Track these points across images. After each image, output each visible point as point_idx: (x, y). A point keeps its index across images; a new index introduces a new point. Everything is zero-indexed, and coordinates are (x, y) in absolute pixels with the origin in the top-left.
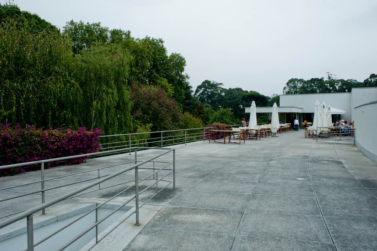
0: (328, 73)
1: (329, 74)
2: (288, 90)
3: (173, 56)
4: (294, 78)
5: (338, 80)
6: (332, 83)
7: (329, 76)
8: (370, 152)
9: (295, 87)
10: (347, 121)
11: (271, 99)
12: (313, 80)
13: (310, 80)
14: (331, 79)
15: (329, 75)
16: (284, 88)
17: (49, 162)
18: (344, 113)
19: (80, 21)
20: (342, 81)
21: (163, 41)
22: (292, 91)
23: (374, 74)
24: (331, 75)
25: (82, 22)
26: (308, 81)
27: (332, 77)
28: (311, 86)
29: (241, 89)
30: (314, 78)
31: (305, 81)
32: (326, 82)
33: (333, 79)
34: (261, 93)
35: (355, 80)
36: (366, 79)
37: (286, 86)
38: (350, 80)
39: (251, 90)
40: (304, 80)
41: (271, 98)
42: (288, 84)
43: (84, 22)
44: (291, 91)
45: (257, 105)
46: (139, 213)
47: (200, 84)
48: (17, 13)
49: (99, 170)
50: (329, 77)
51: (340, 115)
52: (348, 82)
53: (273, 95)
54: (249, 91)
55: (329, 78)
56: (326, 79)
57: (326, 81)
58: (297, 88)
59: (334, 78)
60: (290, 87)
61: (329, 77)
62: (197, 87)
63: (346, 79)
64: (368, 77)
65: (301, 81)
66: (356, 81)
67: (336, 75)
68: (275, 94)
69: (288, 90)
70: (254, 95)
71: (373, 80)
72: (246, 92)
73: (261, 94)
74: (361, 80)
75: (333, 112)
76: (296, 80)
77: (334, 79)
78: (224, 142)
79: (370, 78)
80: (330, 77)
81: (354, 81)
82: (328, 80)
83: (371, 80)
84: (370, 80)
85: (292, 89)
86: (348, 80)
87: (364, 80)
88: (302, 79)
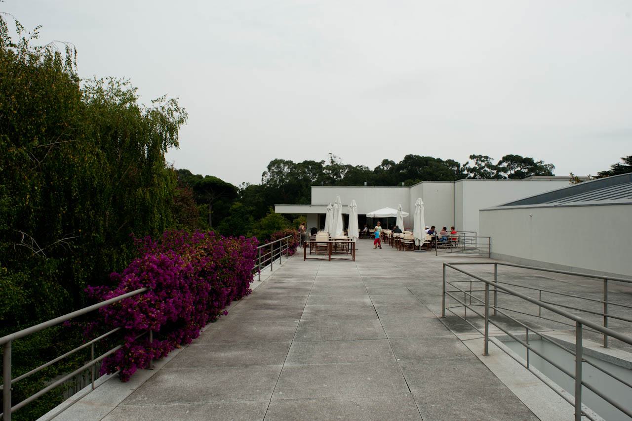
0: (331, 154)
1: (332, 156)
4: (279, 158)
5: (343, 166)
6: (336, 168)
8: (12, 399)
9: (280, 173)
10: (452, 226)
11: (239, 189)
12: (306, 164)
13: (302, 162)
14: (335, 163)
16: (264, 174)
18: (407, 215)
20: (349, 166)
23: (387, 160)
24: (335, 157)
26: (299, 164)
27: (336, 161)
28: (305, 172)
29: (188, 171)
30: (308, 160)
32: (328, 168)
33: (337, 164)
34: (226, 180)
35: (366, 167)
37: (267, 170)
38: (360, 166)
39: (207, 175)
40: (389, 160)
41: (240, 188)
42: (269, 167)
44: (275, 179)
46: (576, 361)
47: (477, 154)
49: (496, 264)
50: (332, 160)
52: (358, 170)
53: (241, 184)
54: (204, 176)
55: (332, 162)
57: (328, 166)
59: (339, 162)
61: (332, 160)
62: (450, 160)
64: (380, 164)
65: (289, 163)
66: (367, 168)
67: (341, 158)
70: (216, 184)
71: (385, 168)
72: (200, 177)
73: (226, 182)
75: (393, 215)
76: (282, 161)
77: (339, 164)
78: (352, 259)
79: (383, 165)
81: (365, 168)
83: (384, 168)
84: (382, 167)
86: (356, 167)
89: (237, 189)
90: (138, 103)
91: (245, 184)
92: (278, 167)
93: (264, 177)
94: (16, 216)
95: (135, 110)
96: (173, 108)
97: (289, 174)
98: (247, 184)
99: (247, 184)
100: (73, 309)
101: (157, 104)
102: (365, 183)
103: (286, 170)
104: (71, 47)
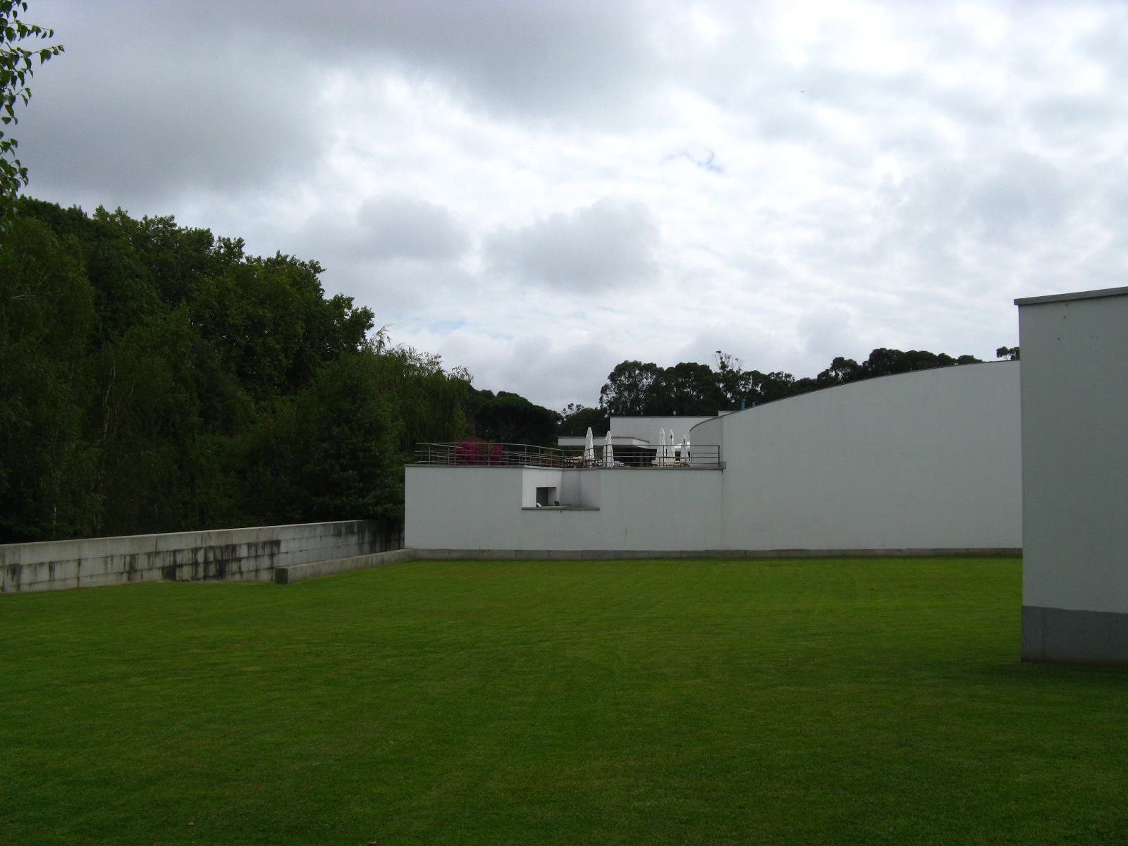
0: (719, 352)
2: (615, 395)
3: (341, 303)
4: (631, 360)
7: (723, 360)
9: (633, 387)
11: (561, 418)
15: (721, 358)
17: (503, 464)
19: (116, 209)
21: (319, 267)
22: (625, 397)
24: (729, 358)
25: (123, 210)
31: (662, 369)
36: (823, 370)
37: (609, 382)
41: (564, 415)
42: (613, 377)
43: (127, 212)
45: (595, 435)
48: (53, 210)
51: (1022, 558)
54: (495, 394)
55: (723, 366)
56: (715, 368)
58: (639, 390)
59: (734, 366)
60: (619, 387)
61: (722, 363)
63: (765, 371)
64: (829, 367)
65: (650, 368)
68: (575, 405)
69: (615, 395)
72: (488, 394)
74: (812, 369)
76: (636, 365)
77: (735, 370)
80: (726, 363)
82: (719, 371)
83: (837, 375)
85: (626, 394)
86: (770, 375)
87: (819, 373)
88: (652, 364)
89: (556, 416)
90: (443, 366)
91: (574, 408)
92: (630, 376)
93: (605, 396)
94: (743, 390)
95: (440, 372)
96: (464, 374)
97: (651, 389)
98: (577, 406)
99: (577, 406)
100: (401, 485)
101: (455, 371)
102: (675, 413)
103: (647, 381)
104: (412, 348)
